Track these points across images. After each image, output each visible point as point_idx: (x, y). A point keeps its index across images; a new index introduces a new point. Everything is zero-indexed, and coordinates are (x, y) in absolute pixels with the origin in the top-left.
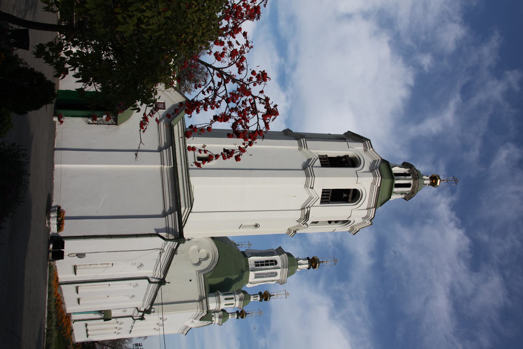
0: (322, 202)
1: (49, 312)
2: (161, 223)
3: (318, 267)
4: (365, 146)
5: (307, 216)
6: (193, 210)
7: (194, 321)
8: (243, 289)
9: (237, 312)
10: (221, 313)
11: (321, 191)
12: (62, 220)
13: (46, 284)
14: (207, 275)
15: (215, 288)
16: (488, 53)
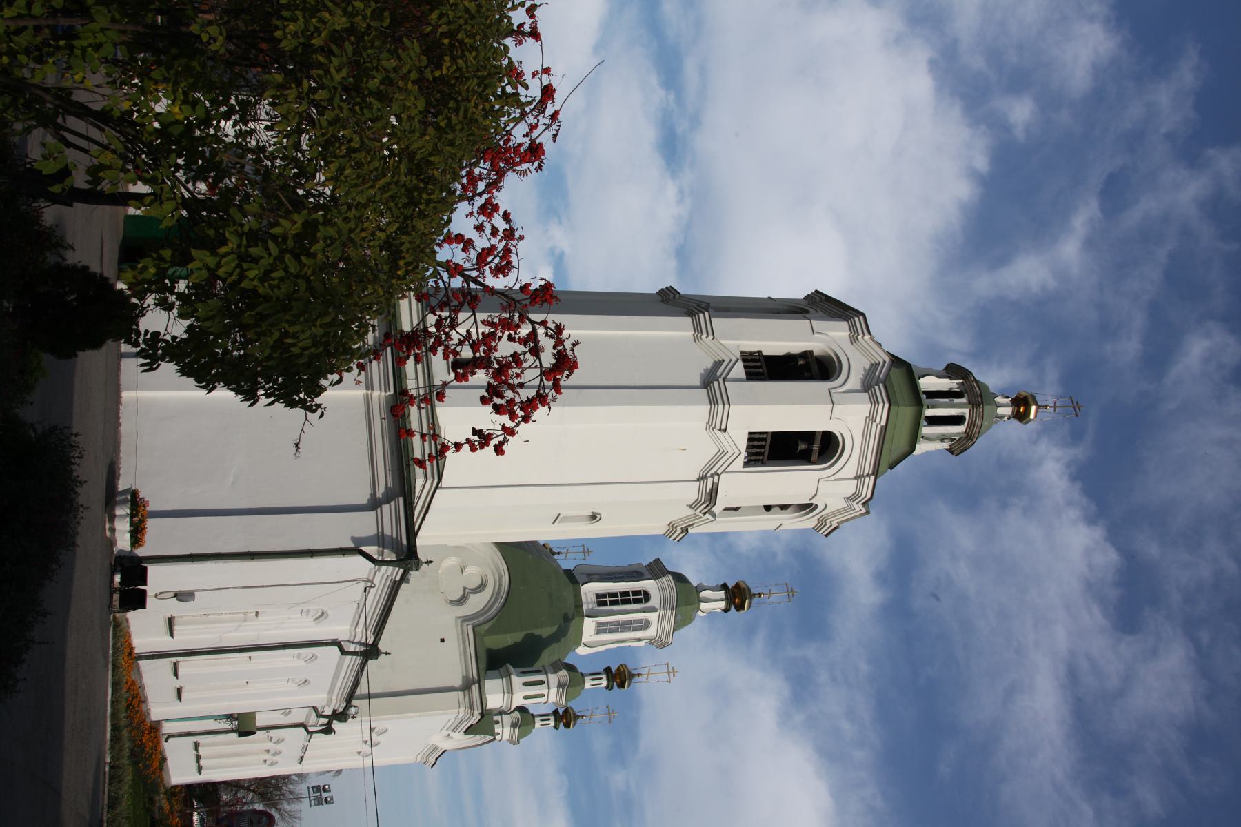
0: (746, 464)
1: (115, 728)
2: (365, 524)
3: (749, 607)
4: (853, 329)
5: (712, 496)
6: (444, 483)
7: (452, 734)
8: (567, 661)
9: (555, 712)
10: (517, 714)
11: (746, 437)
12: (142, 521)
13: (107, 666)
14: (481, 627)
15: (496, 661)
16: (1168, 101)
